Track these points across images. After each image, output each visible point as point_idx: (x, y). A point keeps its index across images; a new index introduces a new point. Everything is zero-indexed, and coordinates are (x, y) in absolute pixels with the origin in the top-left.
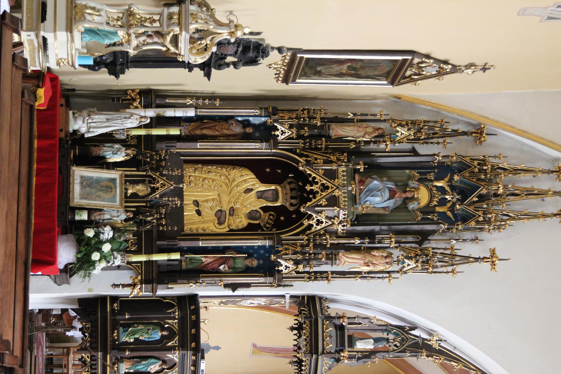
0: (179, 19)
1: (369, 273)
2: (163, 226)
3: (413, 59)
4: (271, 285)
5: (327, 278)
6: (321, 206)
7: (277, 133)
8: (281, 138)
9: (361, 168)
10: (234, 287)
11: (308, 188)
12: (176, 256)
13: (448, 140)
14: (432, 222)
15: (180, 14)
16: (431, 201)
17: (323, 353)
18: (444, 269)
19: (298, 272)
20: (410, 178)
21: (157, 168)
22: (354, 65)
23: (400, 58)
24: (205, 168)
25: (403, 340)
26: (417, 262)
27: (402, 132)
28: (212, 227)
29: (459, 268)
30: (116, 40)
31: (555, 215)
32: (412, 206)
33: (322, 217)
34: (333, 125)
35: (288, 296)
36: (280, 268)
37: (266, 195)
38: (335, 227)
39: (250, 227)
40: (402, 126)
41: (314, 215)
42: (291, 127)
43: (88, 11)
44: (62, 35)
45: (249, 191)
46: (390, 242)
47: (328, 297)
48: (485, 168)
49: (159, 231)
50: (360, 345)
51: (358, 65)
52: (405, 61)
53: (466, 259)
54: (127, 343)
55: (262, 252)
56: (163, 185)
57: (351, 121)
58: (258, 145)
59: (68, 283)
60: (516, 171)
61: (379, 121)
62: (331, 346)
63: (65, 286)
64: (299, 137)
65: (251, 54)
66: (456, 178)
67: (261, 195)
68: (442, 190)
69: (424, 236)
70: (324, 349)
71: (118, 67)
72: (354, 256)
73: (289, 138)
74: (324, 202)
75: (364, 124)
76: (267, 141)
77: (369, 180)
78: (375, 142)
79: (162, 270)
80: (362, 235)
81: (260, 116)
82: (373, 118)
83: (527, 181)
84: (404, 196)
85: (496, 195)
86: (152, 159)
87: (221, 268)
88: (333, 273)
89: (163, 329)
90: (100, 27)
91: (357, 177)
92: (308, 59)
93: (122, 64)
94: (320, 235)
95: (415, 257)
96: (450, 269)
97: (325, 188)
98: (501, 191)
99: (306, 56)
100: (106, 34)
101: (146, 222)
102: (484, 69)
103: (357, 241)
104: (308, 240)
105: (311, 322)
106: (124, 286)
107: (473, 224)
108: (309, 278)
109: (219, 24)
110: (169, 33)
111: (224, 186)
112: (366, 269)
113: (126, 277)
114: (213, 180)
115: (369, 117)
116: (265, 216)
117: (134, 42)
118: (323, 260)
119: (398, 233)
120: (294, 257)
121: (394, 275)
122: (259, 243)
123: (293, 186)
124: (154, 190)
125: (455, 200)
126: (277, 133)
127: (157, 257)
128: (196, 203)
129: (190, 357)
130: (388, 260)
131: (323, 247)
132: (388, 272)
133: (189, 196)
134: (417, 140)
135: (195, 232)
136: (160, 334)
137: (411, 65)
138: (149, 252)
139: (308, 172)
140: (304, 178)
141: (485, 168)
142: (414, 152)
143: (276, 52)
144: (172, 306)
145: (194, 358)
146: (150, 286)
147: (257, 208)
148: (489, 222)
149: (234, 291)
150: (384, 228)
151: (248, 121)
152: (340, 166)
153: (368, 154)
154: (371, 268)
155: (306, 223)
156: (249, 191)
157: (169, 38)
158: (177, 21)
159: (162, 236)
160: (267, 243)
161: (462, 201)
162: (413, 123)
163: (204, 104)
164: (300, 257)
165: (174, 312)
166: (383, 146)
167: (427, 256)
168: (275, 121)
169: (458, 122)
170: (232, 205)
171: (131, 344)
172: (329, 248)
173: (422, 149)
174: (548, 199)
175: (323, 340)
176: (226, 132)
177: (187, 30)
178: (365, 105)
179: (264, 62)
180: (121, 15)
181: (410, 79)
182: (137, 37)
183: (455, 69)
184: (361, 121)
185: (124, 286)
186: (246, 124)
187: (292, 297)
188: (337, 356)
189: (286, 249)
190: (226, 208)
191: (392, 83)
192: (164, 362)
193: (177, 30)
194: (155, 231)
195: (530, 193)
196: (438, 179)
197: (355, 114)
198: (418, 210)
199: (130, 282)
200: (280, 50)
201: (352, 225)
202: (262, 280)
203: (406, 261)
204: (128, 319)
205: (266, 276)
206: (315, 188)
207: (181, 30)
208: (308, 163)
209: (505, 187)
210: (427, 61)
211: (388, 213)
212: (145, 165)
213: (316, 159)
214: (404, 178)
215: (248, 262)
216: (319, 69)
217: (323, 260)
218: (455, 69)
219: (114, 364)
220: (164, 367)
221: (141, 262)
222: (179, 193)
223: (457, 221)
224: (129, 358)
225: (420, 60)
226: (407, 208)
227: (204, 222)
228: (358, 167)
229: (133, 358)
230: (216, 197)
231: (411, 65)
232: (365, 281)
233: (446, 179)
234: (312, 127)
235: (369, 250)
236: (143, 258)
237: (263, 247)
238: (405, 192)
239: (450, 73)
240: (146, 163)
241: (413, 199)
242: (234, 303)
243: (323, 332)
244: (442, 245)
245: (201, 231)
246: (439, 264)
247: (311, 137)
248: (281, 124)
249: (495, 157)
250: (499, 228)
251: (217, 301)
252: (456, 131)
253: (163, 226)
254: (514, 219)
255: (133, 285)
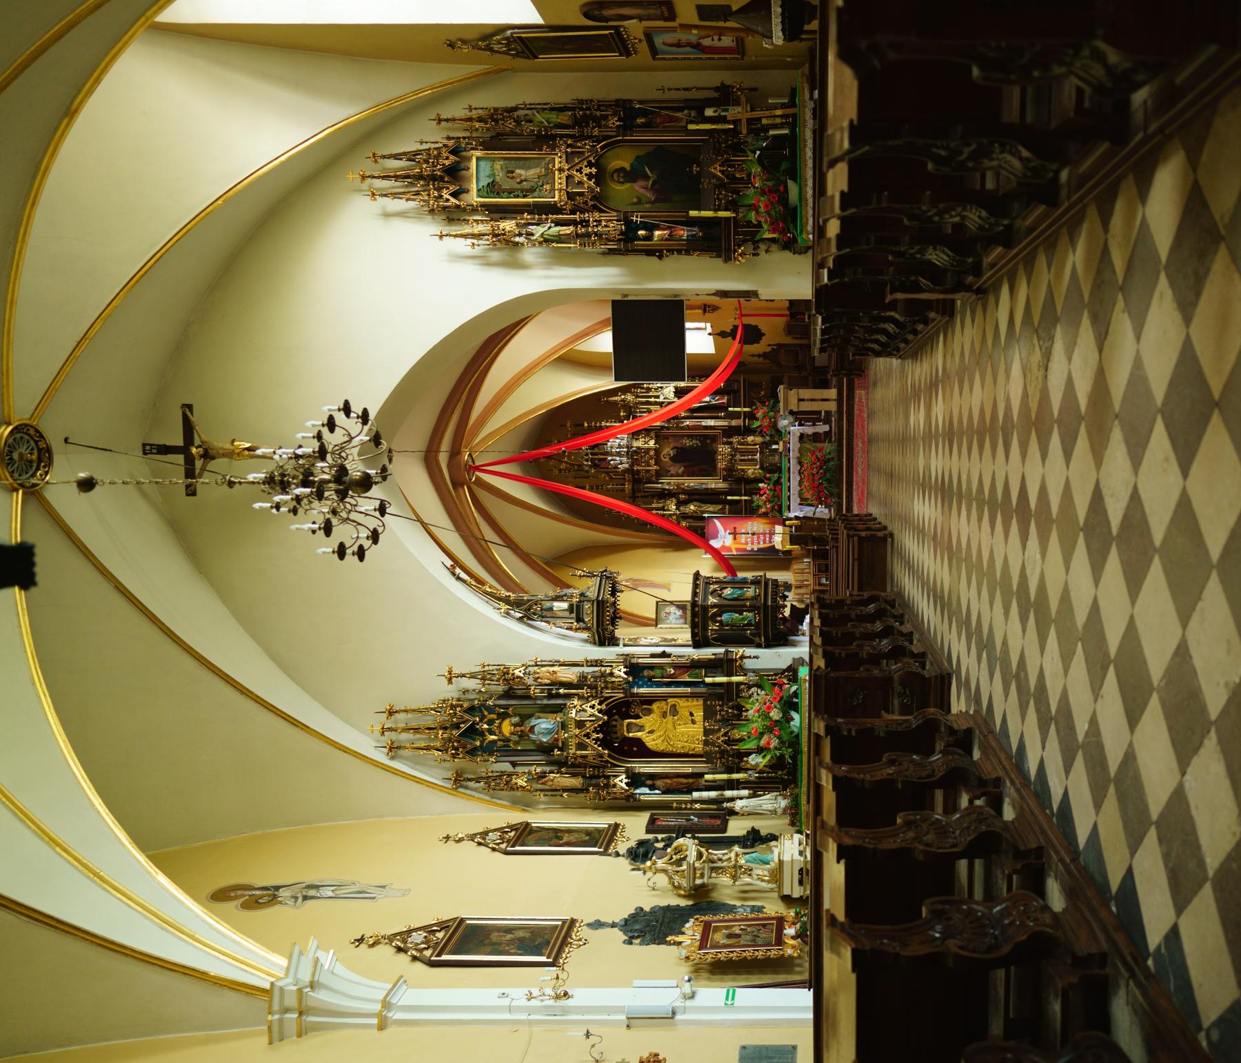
0: (695, 874)
1: (553, 665)
2: (719, 705)
3: (507, 847)
4: (633, 656)
5: (587, 662)
6: (591, 721)
7: (626, 781)
8: (623, 776)
9: (556, 752)
10: (664, 655)
11: (600, 736)
12: (708, 680)
13: (484, 775)
14: (500, 706)
15: (694, 878)
16: (501, 723)
17: (593, 601)
18: (491, 668)
19: (612, 666)
20: (517, 743)
21: (723, 753)
22: (557, 841)
23: (517, 848)
24: (686, 750)
25: (529, 610)
26: (513, 674)
27: (521, 782)
28: (682, 703)
29: (479, 669)
30: (747, 857)
31: (396, 712)
32: (516, 720)
33: (590, 711)
34: (579, 787)
35: (621, 646)
36: (625, 670)
37: (638, 728)
38: (580, 703)
39: (650, 702)
40: (521, 787)
41: (596, 713)
42: (615, 786)
43: (767, 878)
44: (787, 858)
45: (651, 732)
46: (535, 691)
47: (589, 645)
48: (453, 752)
49: (722, 700)
50: (565, 605)
51: (554, 841)
52: (513, 846)
53: (473, 676)
54: (749, 611)
55: (640, 683)
56: (718, 738)
57: (565, 790)
58: (642, 770)
59: (794, 659)
60: (427, 748)
61: (541, 790)
62: (587, 606)
63: (797, 657)
64: (608, 777)
65: (641, 850)
66: (478, 743)
67: (641, 728)
68: (491, 732)
69: (508, 695)
70: (593, 604)
71: (751, 837)
72: (564, 679)
73: (616, 776)
74: (588, 724)
75: (553, 787)
76: (634, 774)
77: (551, 742)
78: (545, 773)
79: (720, 670)
80: (558, 696)
81: (640, 794)
82: (547, 793)
83: (419, 739)
84: (523, 728)
85: (445, 728)
86: (728, 759)
87: (673, 671)
88: (583, 666)
89: (721, 622)
90: (758, 866)
91: (560, 745)
92: (595, 846)
93: (748, 840)
94: (592, 696)
95: (514, 679)
96: (486, 668)
97: (587, 736)
98: (440, 732)
99: (596, 849)
100: (754, 861)
101: (732, 708)
102: (447, 838)
103: (562, 691)
104: (602, 693)
105: (603, 626)
106: (750, 657)
107: (466, 705)
108: (602, 662)
109: (664, 871)
110: (704, 862)
111: (671, 736)
112: (555, 669)
113: (748, 664)
114: (680, 741)
115: (550, 793)
116: (638, 711)
117: (733, 855)
118: (589, 677)
119: (528, 697)
120: (613, 679)
121: (533, 663)
122: (642, 690)
123: (615, 736)
124: (725, 734)
125: (481, 724)
126: (626, 781)
127: (723, 679)
128: (693, 722)
129: (699, 600)
130: (537, 676)
131: (589, 687)
132: (537, 665)
133: (697, 730)
134: (510, 775)
135: (695, 699)
136: (723, 618)
137: (508, 841)
138: (730, 684)
139: (600, 748)
140: (604, 743)
141: (453, 752)
142: (514, 764)
143: (621, 853)
144: (713, 639)
145: (697, 599)
146: (729, 657)
147: (644, 718)
148: (453, 707)
149: (664, 652)
150: (539, 702)
151: (651, 790)
152: (573, 754)
153: (549, 763)
154: (551, 669)
155: (604, 707)
156: (651, 732)
157: (704, 858)
158: (697, 872)
159: (719, 697)
160: (635, 690)
161: (474, 723)
162: (512, 789)
163: (686, 804)
164: (609, 679)
165: (712, 635)
166: (539, 770)
167: (505, 679)
168: (626, 791)
169: (475, 790)
170: (664, 720)
171: (746, 611)
172: (586, 685)
173: (507, 767)
174: (402, 725)
175: (593, 611)
176: (668, 781)
177: (689, 864)
178: (555, 803)
179: (633, 843)
180: (742, 876)
181: (512, 828)
182: (730, 858)
183: (472, 838)
184: (556, 790)
185: (750, 657)
186: (652, 787)
187: (618, 645)
188: (582, 599)
189: (620, 685)
190: (670, 718)
191: (528, 824)
192: (720, 596)
193: (697, 865)
194: (725, 701)
195: (416, 730)
196: (494, 742)
197: (562, 796)
198: (512, 716)
199: (745, 660)
200: (617, 854)
201: (565, 704)
202: (640, 661)
203: (522, 675)
204: (748, 630)
205: (637, 664)
206: (595, 736)
207: (694, 864)
208: (601, 756)
209: (436, 737)
210: (494, 846)
211: (537, 714)
212: (733, 755)
213: (594, 759)
214: (522, 742)
215: (652, 673)
216: (587, 838)
217: (589, 677)
218: (472, 838)
219: (759, 595)
220: (720, 592)
221: (737, 676)
222: (707, 732)
223: (479, 707)
224: (747, 599)
225: (501, 846)
226: (521, 718)
227: (688, 707)
228: (559, 753)
229: (744, 600)
230: (677, 727)
231: (508, 841)
232: (556, 659)
233: (487, 741)
234: (596, 786)
235: (553, 684)
236: (735, 679)
237: (639, 687)
238: (522, 731)
239: (476, 835)
240: (733, 756)
241: (515, 725)
242: (665, 640)
243: (593, 618)
244: (493, 688)
245: (690, 699)
246: (496, 672)
247: (598, 777)
248: (622, 788)
249: (445, 761)
250: (444, 701)
251: (680, 642)
252: (477, 782)
253: (719, 705)
254: (432, 709)
255: (743, 657)
